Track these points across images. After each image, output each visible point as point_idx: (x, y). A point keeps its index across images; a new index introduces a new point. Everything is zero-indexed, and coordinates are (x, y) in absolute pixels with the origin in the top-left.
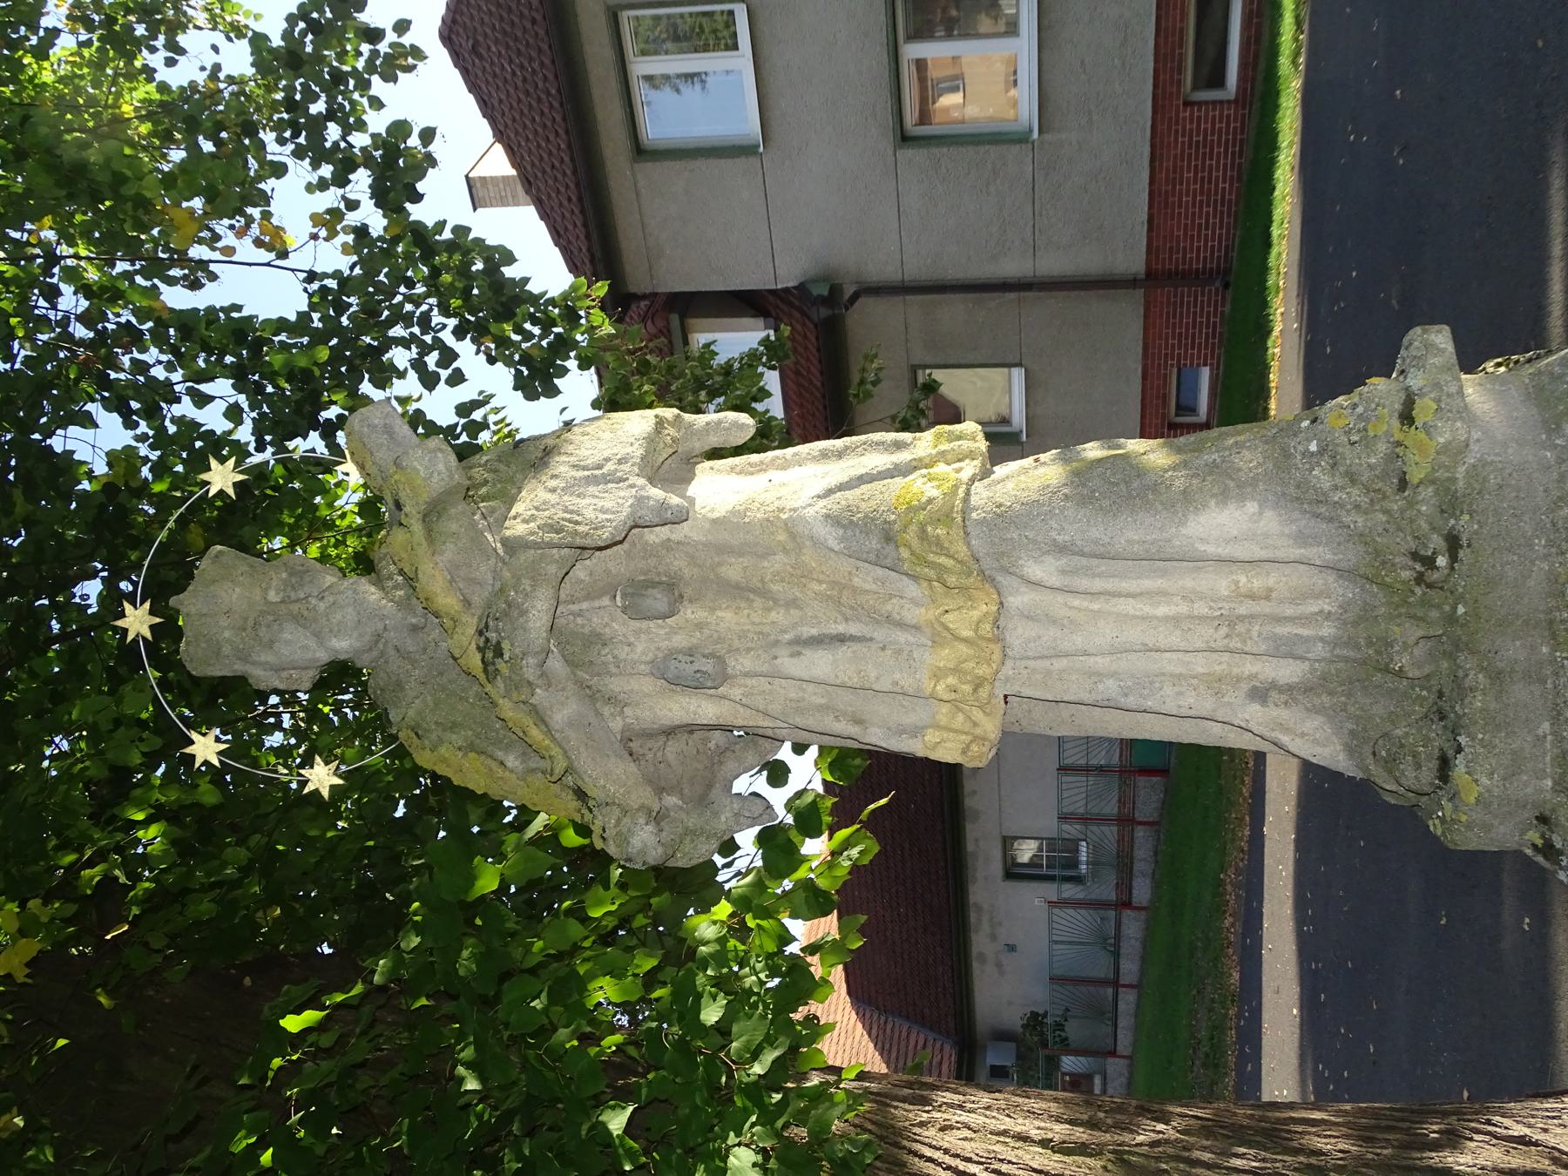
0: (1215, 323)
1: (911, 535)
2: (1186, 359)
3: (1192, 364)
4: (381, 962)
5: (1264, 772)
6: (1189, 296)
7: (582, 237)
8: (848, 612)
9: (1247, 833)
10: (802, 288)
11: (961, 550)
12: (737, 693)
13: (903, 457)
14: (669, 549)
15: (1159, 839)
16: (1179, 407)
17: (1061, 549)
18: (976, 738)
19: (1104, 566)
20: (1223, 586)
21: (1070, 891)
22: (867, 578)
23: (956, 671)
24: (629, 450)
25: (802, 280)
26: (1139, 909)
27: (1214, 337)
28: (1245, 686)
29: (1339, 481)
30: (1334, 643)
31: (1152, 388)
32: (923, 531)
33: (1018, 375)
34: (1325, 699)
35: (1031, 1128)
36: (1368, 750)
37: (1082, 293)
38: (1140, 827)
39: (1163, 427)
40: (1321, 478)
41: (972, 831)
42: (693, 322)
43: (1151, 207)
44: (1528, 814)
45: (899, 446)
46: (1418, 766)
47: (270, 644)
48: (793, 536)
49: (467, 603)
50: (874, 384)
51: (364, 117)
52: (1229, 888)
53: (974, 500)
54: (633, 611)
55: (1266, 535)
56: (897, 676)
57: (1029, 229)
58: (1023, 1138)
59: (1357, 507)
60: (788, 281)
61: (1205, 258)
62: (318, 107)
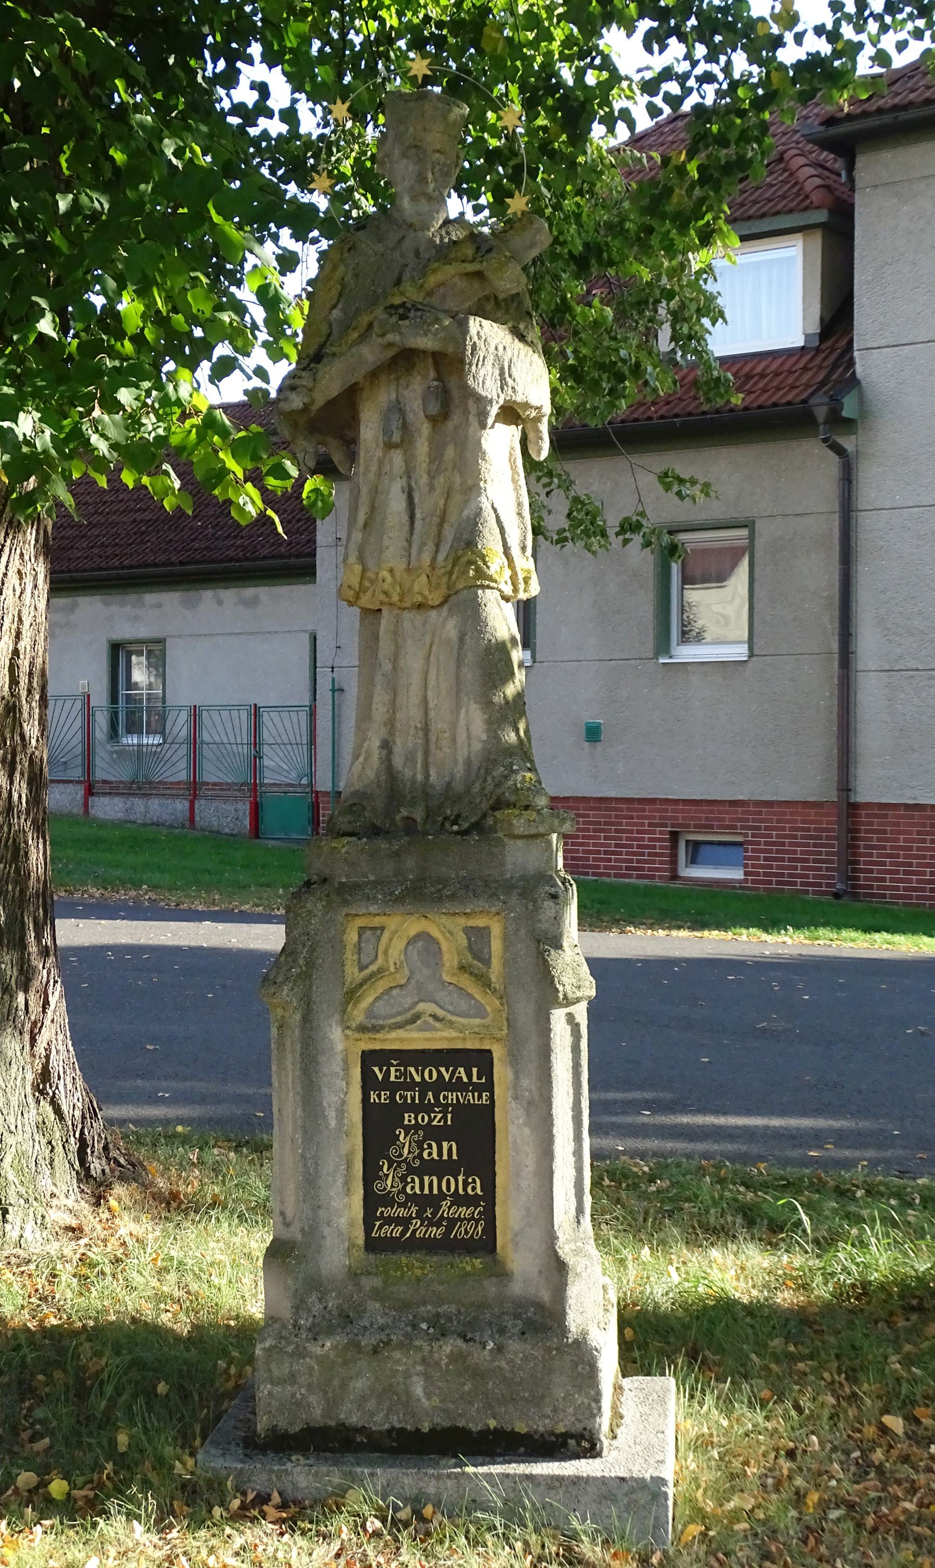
0: (795, 884)
2: (753, 851)
3: (746, 858)
5: (269, 922)
6: (827, 853)
9: (200, 908)
10: (854, 382)
13: (515, 551)
15: (172, 827)
16: (697, 844)
17: (462, 638)
21: (102, 721)
22: (449, 534)
24: (520, 393)
25: (863, 382)
26: (86, 804)
27: (778, 883)
29: (497, 780)
31: (720, 812)
33: (739, 652)
34: (383, 778)
35: (25, 643)
36: (357, 801)
38: (187, 804)
39: (673, 826)
42: (817, 240)
44: (327, 872)
45: (524, 549)
46: (350, 823)
47: (404, 155)
48: (470, 489)
49: (430, 294)
50: (679, 493)
51: (891, 31)
52: (133, 893)
53: (488, 591)
55: (469, 745)
56: (391, 549)
59: (483, 789)
61: (871, 871)
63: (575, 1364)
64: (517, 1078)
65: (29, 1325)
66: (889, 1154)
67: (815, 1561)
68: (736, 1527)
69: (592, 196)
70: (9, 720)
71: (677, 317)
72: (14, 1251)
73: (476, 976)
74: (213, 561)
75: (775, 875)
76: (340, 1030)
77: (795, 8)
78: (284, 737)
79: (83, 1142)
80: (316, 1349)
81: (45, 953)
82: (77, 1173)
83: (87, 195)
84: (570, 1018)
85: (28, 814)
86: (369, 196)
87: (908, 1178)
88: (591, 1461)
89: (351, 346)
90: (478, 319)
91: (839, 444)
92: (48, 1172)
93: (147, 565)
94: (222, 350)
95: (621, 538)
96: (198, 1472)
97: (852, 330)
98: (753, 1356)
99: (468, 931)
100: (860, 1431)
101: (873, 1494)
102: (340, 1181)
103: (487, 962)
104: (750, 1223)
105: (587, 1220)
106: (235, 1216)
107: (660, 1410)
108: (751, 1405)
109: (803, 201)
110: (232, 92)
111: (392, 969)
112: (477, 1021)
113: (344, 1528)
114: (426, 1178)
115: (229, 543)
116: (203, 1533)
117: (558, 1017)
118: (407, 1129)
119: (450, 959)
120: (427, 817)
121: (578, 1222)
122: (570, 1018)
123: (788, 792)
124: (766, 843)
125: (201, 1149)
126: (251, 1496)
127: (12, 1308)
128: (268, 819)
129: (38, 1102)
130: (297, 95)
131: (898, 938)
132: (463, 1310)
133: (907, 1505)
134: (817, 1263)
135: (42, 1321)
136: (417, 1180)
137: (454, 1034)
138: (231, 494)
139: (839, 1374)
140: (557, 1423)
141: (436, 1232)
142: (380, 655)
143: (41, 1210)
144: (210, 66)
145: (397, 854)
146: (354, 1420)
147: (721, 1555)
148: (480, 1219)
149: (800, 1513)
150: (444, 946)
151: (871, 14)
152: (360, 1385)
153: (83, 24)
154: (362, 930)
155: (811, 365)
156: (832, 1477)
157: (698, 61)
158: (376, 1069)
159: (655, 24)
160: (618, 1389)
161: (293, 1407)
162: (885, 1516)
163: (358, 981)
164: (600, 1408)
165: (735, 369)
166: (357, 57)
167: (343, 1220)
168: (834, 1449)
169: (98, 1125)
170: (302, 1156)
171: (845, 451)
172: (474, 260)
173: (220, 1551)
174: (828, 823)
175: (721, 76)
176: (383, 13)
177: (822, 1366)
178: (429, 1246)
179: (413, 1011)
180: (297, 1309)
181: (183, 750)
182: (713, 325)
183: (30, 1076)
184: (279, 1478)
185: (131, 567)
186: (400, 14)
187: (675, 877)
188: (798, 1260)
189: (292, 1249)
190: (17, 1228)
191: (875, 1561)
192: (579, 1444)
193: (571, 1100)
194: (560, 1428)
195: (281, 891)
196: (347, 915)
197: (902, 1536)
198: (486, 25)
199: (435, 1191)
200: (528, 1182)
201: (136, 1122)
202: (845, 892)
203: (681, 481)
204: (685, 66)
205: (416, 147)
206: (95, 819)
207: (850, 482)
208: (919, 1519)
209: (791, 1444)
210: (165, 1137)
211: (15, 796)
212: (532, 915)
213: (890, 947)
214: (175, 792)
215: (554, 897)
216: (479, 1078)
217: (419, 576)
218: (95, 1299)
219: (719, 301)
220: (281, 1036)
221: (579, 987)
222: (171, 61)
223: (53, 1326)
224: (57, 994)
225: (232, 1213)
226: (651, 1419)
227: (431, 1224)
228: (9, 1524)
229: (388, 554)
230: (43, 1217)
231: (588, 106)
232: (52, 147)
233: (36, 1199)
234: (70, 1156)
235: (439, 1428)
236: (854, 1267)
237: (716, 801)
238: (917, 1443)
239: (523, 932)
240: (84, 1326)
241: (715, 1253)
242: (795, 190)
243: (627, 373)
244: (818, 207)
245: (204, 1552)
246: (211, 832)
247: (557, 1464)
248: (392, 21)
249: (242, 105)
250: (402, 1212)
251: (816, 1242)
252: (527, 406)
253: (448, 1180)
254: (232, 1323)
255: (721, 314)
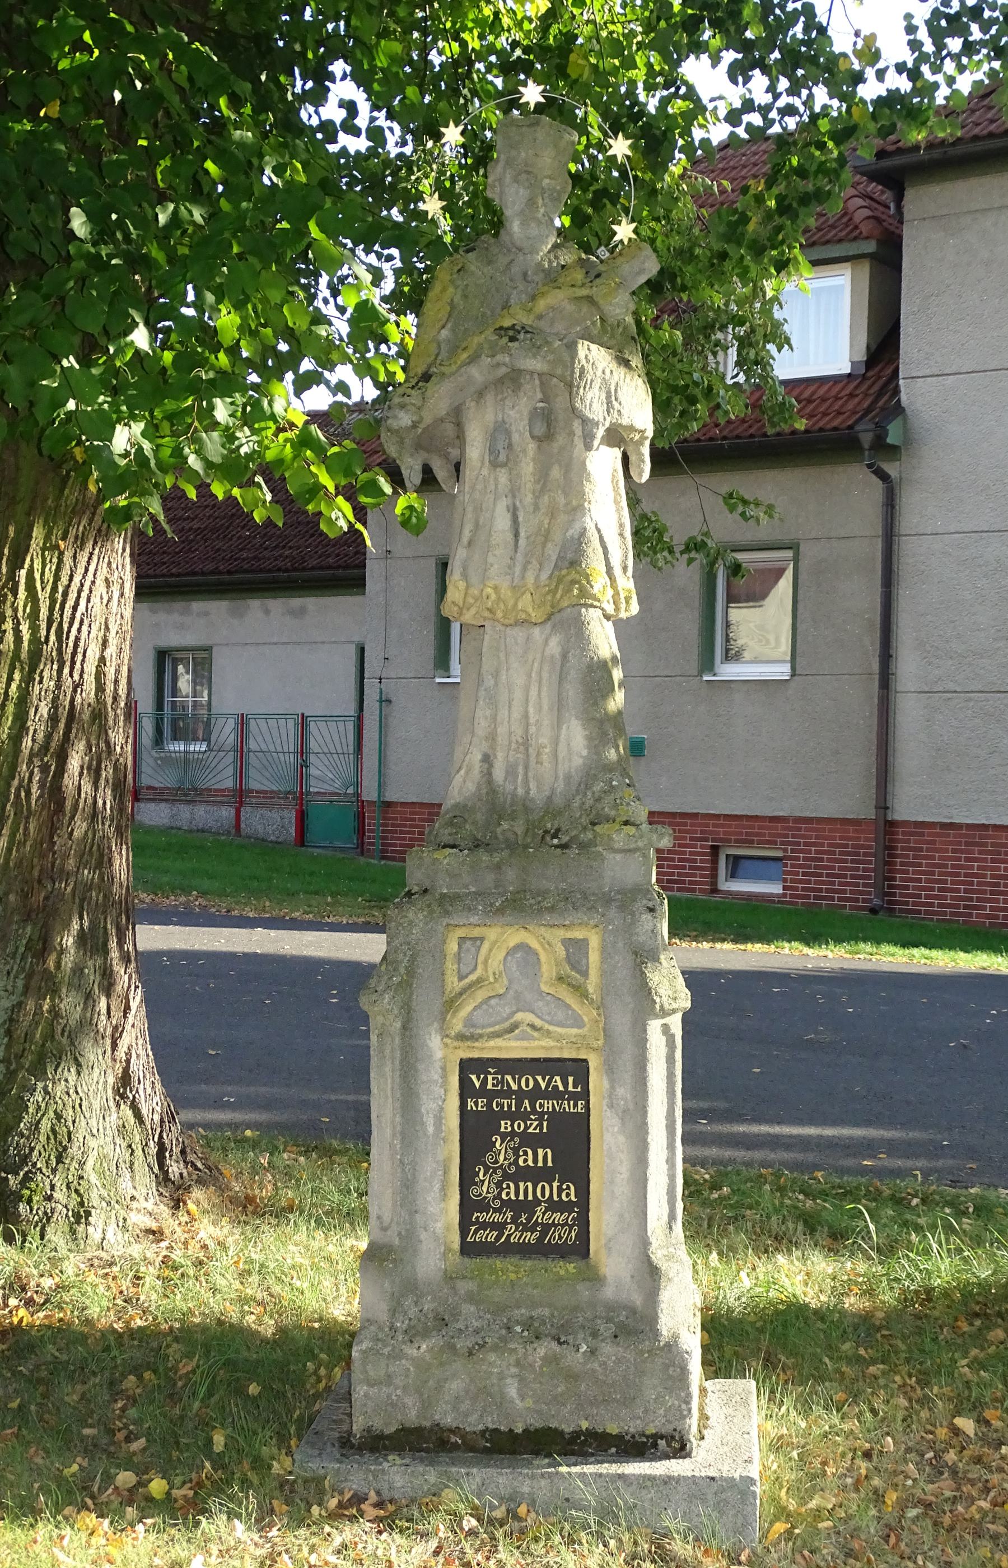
0: (832, 899)
1: (573, 575)
4: (250, 134)
7: (977, 131)
8: (532, 539)
9: (251, 915)
10: (899, 410)
11: (565, 603)
12: (485, 472)
13: (618, 571)
14: (569, 434)
16: (737, 859)
17: (564, 656)
18: (461, 609)
19: (555, 678)
20: (543, 740)
22: (552, 552)
23: (499, 598)
24: (626, 416)
25: (908, 411)
28: (490, 752)
29: (596, 796)
30: (514, 795)
32: (576, 582)
33: (781, 671)
34: (485, 791)
35: (111, 651)
36: (458, 813)
37: (874, 748)
38: (233, 812)
39: (713, 840)
40: (599, 786)
41: (218, 608)
42: (865, 269)
43: (970, 826)
44: (427, 884)
45: (625, 569)
46: (450, 835)
47: (516, 180)
49: (540, 317)
50: (743, 514)
51: (967, 72)
52: (183, 899)
53: (591, 610)
54: (534, 414)
55: (570, 760)
57: (952, 686)
58: (105, 643)
60: (908, 393)
62: (976, 33)
63: (666, 1367)
64: (612, 1088)
65: (115, 1326)
66: (940, 1163)
67: (897, 1559)
68: (820, 1525)
69: (668, 223)
70: (95, 727)
71: (744, 343)
72: (97, 1253)
73: (573, 987)
74: (261, 571)
75: (814, 890)
76: (439, 1038)
77: (877, 44)
78: (338, 747)
79: (161, 1145)
80: (411, 1351)
81: (126, 959)
82: (156, 1176)
83: (186, 208)
84: (666, 1029)
85: (112, 820)
86: (447, 215)
87: (961, 1188)
88: (681, 1461)
89: (461, 367)
90: (586, 343)
91: (883, 471)
92: (128, 1175)
93: (194, 573)
94: (307, 365)
95: (686, 556)
96: (296, 1470)
97: (898, 358)
98: (827, 1360)
99: (567, 943)
100: (932, 1433)
101: (948, 1494)
102: (437, 1187)
103: (585, 974)
104: (812, 1230)
105: (678, 1227)
106: (312, 1222)
107: (744, 1411)
108: (826, 1408)
109: (852, 231)
110: (321, 109)
111: (492, 980)
112: (574, 1031)
113: (441, 1527)
114: (521, 1184)
115: (276, 553)
116: (302, 1532)
117: (654, 1027)
118: (504, 1137)
119: (548, 970)
120: (527, 830)
121: (671, 1228)
122: (666, 1029)
123: (827, 807)
124: (805, 859)
125: (271, 1154)
126: (347, 1496)
127: (98, 1310)
128: (315, 827)
129: (118, 1106)
130: (375, 114)
131: (935, 953)
132: (556, 1313)
133: (983, 1504)
134: (879, 1269)
135: (128, 1323)
136: (512, 1185)
137: (552, 1044)
138: (323, 508)
139: (910, 1376)
140: (647, 1424)
141: (530, 1237)
142: (484, 671)
143: (122, 1213)
144: (299, 83)
145: (498, 867)
146: (449, 1420)
147: (806, 1553)
148: (574, 1225)
149: (879, 1511)
150: (543, 957)
151: (949, 54)
152: (456, 1386)
153: (186, 39)
154: (462, 940)
155: (857, 392)
156: (907, 1477)
157: (781, 94)
158: (474, 1077)
159: (740, 56)
160: (703, 1391)
161: (389, 1408)
162: (962, 1514)
163: (457, 989)
164: (690, 1410)
165: (795, 393)
166: (438, 77)
167: (439, 1225)
168: (908, 1450)
169: (176, 1129)
170: (401, 1161)
171: (889, 477)
172: (583, 285)
173: (321, 1550)
174: (866, 839)
175: (802, 109)
176: (466, 36)
177: (894, 1370)
178: (524, 1250)
179: (512, 1021)
180: (393, 1312)
181: (230, 757)
182: (779, 351)
183: (111, 1080)
184: (375, 1477)
185: (179, 575)
186: (482, 37)
187: (715, 890)
188: (862, 1267)
189: (389, 1253)
190: (100, 1231)
191: (955, 1559)
192: (669, 1445)
193: (664, 1109)
194: (651, 1430)
195: (329, 899)
196: (448, 925)
197: (978, 1535)
198: (572, 51)
199: (530, 1198)
200: (622, 1187)
201: (206, 1126)
202: (882, 907)
203: (745, 502)
204: (766, 99)
205: (528, 173)
206: (141, 825)
207: (893, 507)
208: (994, 1517)
209: (867, 1445)
210: (236, 1141)
211: (100, 802)
212: (629, 929)
213: (928, 962)
214: (219, 799)
215: (652, 910)
216: (575, 1086)
217: (523, 594)
218: (179, 1302)
219: (786, 327)
220: (381, 1044)
221: (675, 999)
222: (263, 78)
223: (139, 1327)
224: (138, 999)
225: (310, 1216)
226: (735, 1420)
227: (525, 1229)
228: (111, 1523)
229: (493, 572)
230: (125, 1220)
231: (669, 135)
232: (150, 157)
233: (117, 1202)
234: (150, 1159)
235: (532, 1429)
236: (917, 1274)
237: (736, 816)
238: (989, 1445)
239: (620, 944)
240: (171, 1328)
241: (781, 1259)
242: (845, 220)
243: (700, 396)
244: (867, 238)
245: (306, 1550)
246: (257, 839)
247: (648, 1464)
248: (474, 43)
249: (331, 122)
250: (497, 1217)
251: (879, 1251)
252: (631, 428)
253: (543, 1187)
254: (316, 1325)
255: (788, 341)
